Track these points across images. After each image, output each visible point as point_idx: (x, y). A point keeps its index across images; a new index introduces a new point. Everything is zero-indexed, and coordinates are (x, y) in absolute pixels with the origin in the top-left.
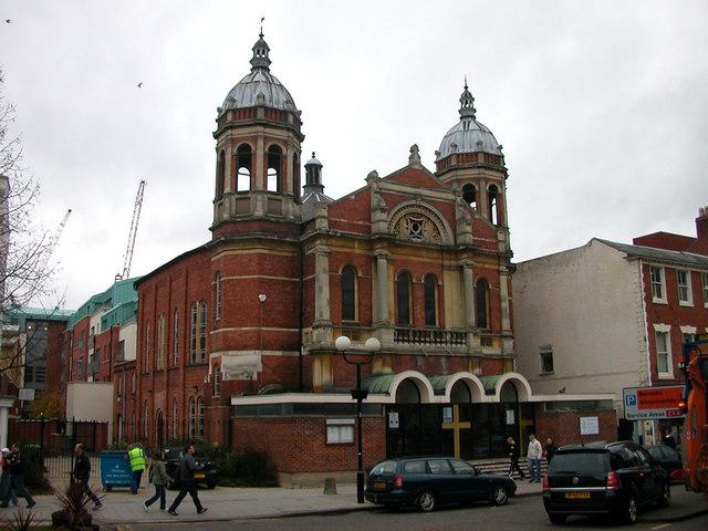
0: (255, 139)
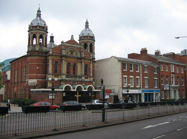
0: (37, 33)
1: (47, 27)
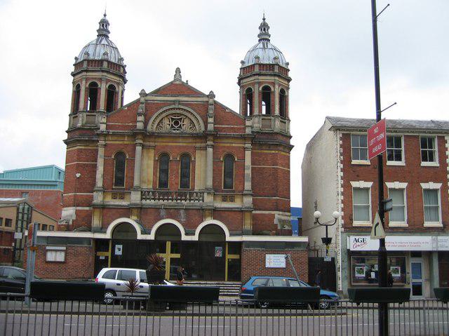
0: (273, 84)
1: (288, 64)
